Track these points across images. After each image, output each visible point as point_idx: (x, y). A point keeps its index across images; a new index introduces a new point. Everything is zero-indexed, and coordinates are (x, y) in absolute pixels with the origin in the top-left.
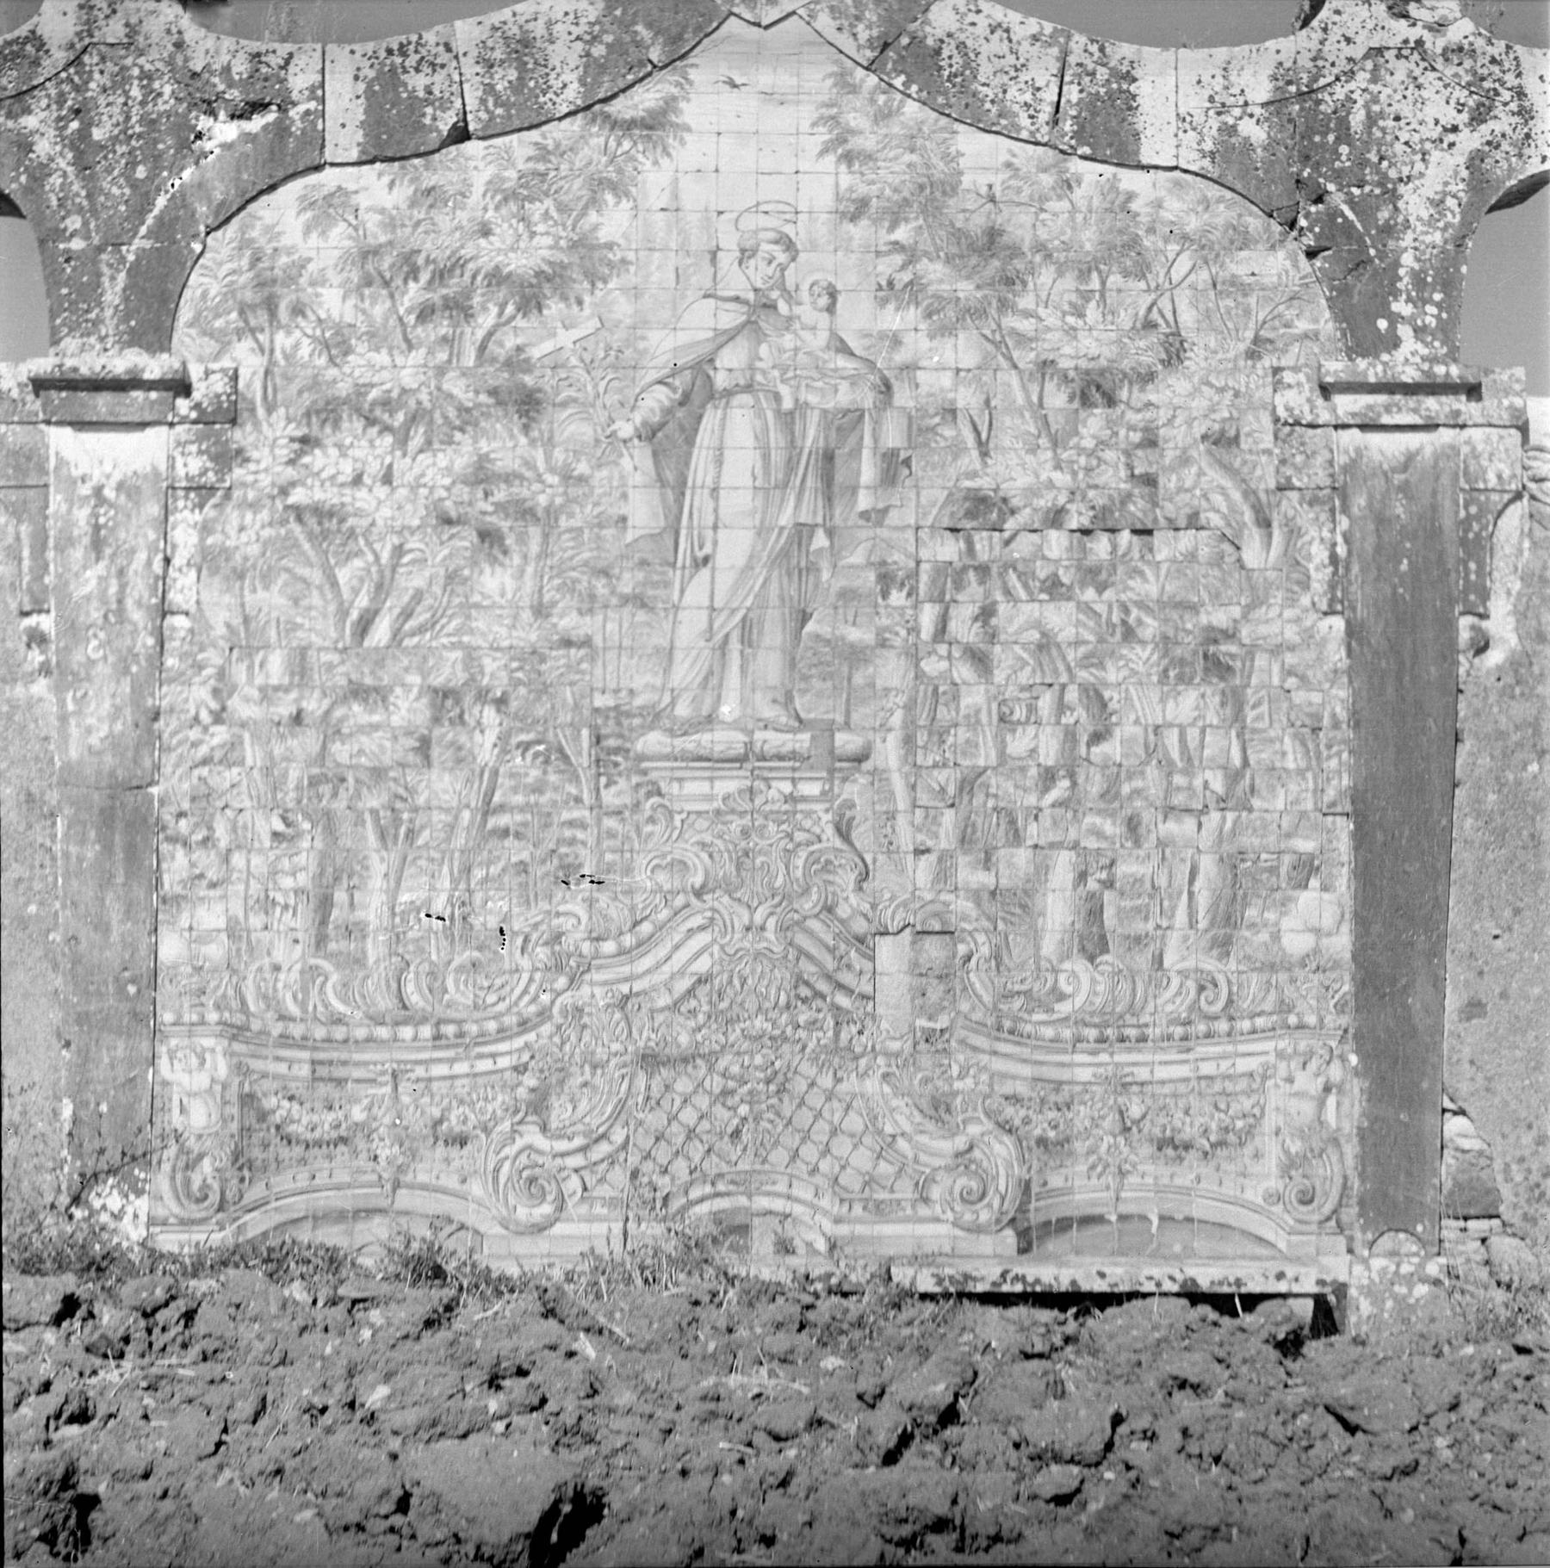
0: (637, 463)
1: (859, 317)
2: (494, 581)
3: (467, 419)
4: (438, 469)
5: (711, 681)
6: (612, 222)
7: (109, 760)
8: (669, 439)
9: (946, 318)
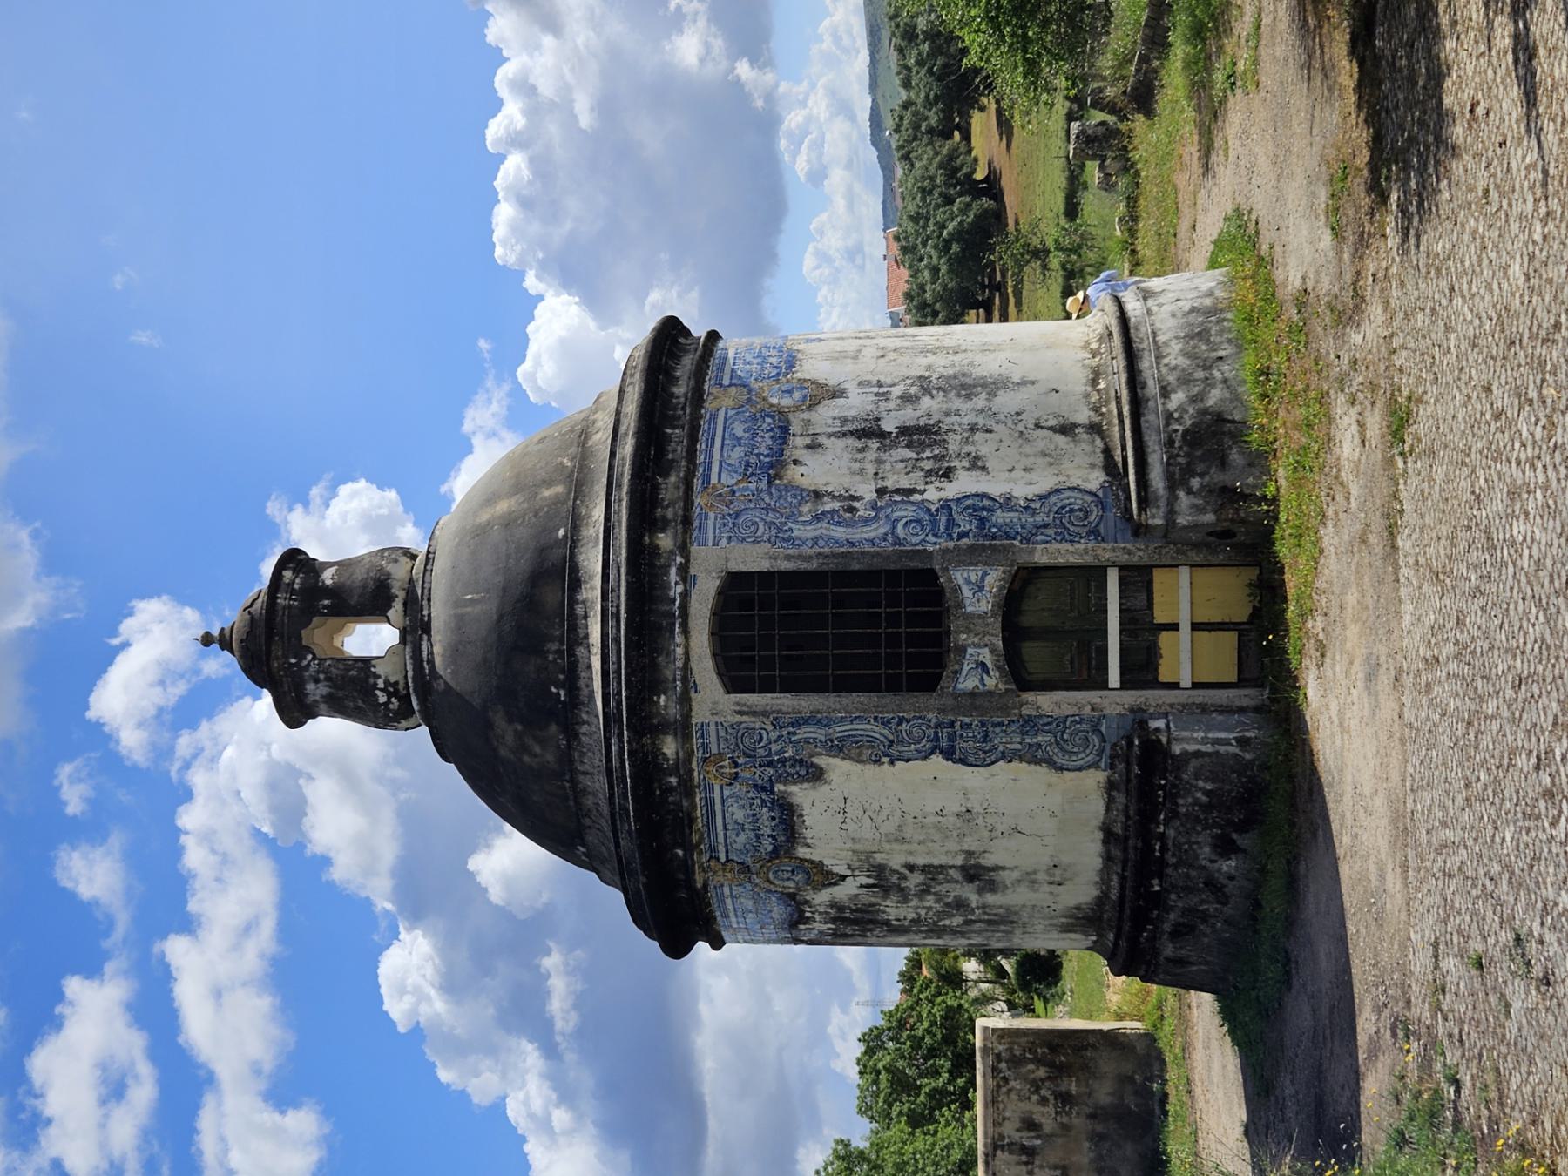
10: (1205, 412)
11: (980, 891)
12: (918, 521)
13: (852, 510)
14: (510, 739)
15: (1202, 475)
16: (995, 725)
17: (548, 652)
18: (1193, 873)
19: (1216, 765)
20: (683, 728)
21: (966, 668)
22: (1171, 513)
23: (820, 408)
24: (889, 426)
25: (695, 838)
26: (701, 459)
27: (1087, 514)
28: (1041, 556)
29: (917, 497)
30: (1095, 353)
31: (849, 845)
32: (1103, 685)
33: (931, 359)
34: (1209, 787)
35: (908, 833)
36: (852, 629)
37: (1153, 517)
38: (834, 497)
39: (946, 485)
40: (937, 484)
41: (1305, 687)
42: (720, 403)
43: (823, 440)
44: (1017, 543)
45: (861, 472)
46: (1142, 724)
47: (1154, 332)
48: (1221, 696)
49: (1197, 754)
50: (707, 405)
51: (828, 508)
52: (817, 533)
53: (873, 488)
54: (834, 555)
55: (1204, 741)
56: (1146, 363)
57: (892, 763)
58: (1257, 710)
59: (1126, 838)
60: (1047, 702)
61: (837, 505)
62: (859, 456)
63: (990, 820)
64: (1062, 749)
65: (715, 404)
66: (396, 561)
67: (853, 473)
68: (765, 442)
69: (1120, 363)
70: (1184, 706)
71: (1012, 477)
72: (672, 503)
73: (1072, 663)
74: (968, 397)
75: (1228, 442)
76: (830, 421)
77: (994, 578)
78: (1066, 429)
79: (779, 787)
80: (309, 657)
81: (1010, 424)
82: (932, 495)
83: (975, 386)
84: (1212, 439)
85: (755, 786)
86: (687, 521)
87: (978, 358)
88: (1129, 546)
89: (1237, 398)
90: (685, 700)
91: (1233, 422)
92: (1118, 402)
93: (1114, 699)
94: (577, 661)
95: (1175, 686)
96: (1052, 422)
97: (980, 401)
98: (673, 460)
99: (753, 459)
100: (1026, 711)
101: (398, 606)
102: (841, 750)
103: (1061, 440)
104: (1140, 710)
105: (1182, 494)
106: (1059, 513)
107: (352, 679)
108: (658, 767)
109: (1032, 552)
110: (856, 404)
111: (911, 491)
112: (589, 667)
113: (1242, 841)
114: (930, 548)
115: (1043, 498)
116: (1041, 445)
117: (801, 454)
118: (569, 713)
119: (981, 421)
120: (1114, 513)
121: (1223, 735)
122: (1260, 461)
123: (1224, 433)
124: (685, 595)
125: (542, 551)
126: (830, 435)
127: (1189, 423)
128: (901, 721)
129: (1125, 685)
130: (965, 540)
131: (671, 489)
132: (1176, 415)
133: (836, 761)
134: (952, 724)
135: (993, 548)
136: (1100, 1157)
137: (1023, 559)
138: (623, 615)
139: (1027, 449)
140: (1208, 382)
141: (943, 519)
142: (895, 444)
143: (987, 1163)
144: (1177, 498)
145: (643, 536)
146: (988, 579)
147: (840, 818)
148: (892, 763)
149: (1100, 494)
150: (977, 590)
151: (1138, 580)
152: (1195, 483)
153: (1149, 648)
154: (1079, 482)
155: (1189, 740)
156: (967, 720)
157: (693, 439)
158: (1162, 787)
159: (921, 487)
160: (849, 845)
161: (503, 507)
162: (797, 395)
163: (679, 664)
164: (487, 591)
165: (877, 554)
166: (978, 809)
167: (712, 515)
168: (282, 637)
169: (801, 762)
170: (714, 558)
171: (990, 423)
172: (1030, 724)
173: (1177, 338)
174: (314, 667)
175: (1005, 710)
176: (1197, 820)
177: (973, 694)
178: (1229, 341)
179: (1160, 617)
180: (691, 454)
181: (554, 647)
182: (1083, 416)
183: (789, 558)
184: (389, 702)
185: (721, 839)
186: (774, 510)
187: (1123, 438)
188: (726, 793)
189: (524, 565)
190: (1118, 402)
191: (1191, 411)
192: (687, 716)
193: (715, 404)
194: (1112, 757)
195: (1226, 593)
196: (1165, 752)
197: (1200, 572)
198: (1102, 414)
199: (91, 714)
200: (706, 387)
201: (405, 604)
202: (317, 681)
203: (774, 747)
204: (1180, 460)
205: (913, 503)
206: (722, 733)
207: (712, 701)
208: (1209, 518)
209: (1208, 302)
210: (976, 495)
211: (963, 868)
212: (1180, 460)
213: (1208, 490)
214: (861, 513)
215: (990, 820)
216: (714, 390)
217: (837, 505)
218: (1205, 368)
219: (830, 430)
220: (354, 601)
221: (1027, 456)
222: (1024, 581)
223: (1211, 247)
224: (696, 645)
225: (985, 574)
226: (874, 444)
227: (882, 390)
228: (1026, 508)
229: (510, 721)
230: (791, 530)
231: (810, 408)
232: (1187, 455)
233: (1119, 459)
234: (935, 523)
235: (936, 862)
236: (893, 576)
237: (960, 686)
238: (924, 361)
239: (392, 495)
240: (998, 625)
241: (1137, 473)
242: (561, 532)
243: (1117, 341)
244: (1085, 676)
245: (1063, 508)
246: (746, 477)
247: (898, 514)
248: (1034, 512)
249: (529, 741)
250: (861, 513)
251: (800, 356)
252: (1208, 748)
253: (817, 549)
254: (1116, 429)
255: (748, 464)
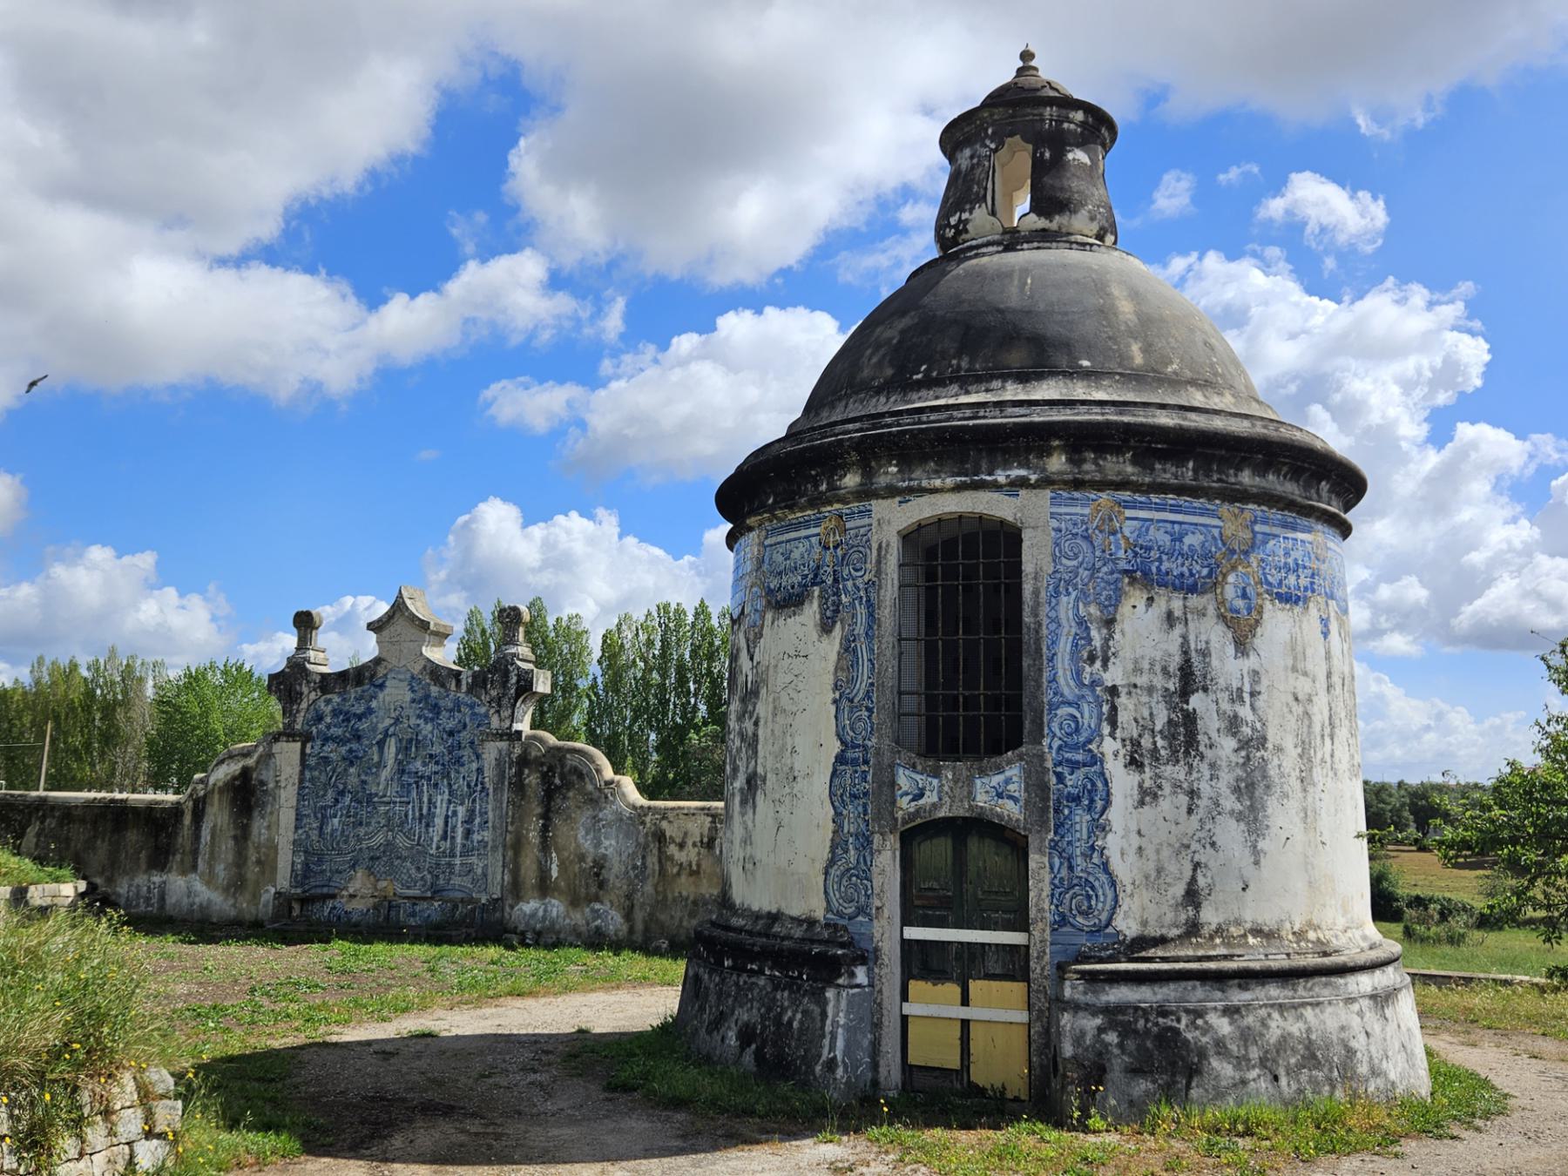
0: (375, 749)
1: (413, 721)
2: (352, 770)
3: (349, 741)
4: (343, 750)
5: (386, 789)
6: (374, 704)
7: (1158, 466)
8: (381, 744)
9: (426, 720)
10: (1202, 1054)
11: (741, 790)
12: (1077, 730)
13: (1092, 659)
14: (888, 334)
15: (1121, 1045)
16: (865, 806)
17: (960, 358)
18: (730, 1001)
19: (813, 1033)
20: (866, 493)
21: (918, 777)
22: (1076, 1007)
23: (1221, 628)
24: (1196, 701)
25: (779, 513)
26: (1155, 498)
27: (1085, 914)
28: (1034, 860)
29: (1106, 729)
30: (1300, 935)
31: (773, 662)
32: (907, 921)
33: (1292, 752)
34: (795, 1024)
35: (780, 719)
36: (969, 661)
37: (1073, 987)
38: (1107, 640)
39: (1121, 760)
40: (1122, 752)
41: (839, 1143)
42: (1228, 521)
43: (1179, 630)
44: (1051, 835)
45: (1137, 670)
46: (862, 960)
47: (1318, 1004)
48: (891, 1045)
49: (824, 1015)
50: (1226, 506)
51: (1094, 633)
52: (1064, 622)
53: (1118, 682)
54: (1038, 641)
55: (835, 1023)
56: (1274, 991)
57: (835, 701)
58: (875, 1083)
59: (767, 936)
60: (887, 863)
61: (1097, 643)
62: (1158, 668)
63: (787, 800)
64: (843, 875)
65: (1226, 514)
66: (1092, 219)
67: (1136, 662)
68: (1172, 566)
69: (1278, 962)
70: (880, 1005)
71: (1132, 835)
72: (1100, 469)
73: (930, 889)
74: (1236, 790)
75: (1163, 1079)
76: (1203, 638)
77: (1011, 810)
78: (1192, 896)
79: (816, 590)
80: (993, 146)
81: (1199, 834)
82: (1109, 746)
83: (1251, 798)
84: (1169, 1062)
85: (818, 567)
86: (1078, 484)
87: (1293, 805)
88: (1047, 958)
89: (1220, 1095)
90: (891, 492)
91: (1188, 1087)
92: (1225, 957)
93: (888, 932)
94: (945, 386)
95: (905, 997)
96: (1201, 882)
97: (1229, 803)
98: (1153, 469)
99: (1154, 554)
100: (877, 838)
101: (1042, 223)
102: (846, 650)
103: (1179, 890)
104: (877, 958)
105: (1098, 1021)
106: (1088, 883)
107: (970, 189)
108: (833, 471)
109: (1041, 851)
110: (1227, 667)
111: (1113, 723)
112: (937, 398)
113: (748, 1058)
114: (1045, 742)
115: (1105, 867)
116: (1172, 868)
117: (1161, 606)
118: (902, 384)
119: (1203, 803)
120: (1084, 943)
121: (840, 1043)
122: (1135, 1115)
123: (1173, 1075)
124: (996, 486)
125: (1066, 346)
126: (1185, 637)
127: (1189, 1036)
128: (869, 710)
129: (907, 945)
130: (1054, 780)
131: (1117, 468)
132: (1200, 1022)
133: (837, 647)
134: (866, 762)
135: (1045, 810)
136: (706, 903)
137: (1033, 842)
138: (971, 423)
139: (1166, 853)
140: (1241, 1062)
141: (1079, 757)
142: (1172, 708)
143: (703, 809)
144: (1094, 1014)
145: (1060, 438)
146: (1010, 804)
147: (792, 653)
148: (835, 701)
149: (1110, 930)
150: (998, 791)
151: (1014, 964)
152: (1112, 1038)
153: (944, 972)
154: (1125, 907)
155: (838, 1006)
156: (869, 778)
157: (1180, 490)
158: (800, 975)
159: (1118, 733)
160: (773, 662)
161: (1126, 308)
162: (1240, 603)
163: (925, 483)
164: (1031, 297)
165: (1039, 686)
166: (797, 787)
167: (1087, 511)
168: (1012, 116)
169: (837, 611)
170: (1040, 518)
171: (1201, 813)
172: (865, 842)
173: (1309, 1030)
174: (984, 152)
175: (878, 817)
176: (769, 1009)
177: (893, 784)
178: (1300, 1091)
179: (975, 986)
180: (1162, 488)
181: (964, 364)
182: (1210, 916)
183: (1036, 593)
184: (951, 227)
185: (780, 538)
186: (1092, 576)
187: (1177, 960)
188: (813, 540)
189: (1052, 329)
190: (1225, 957)
191: (1204, 1040)
192: (876, 495)
193: (1226, 514)
194: (835, 925)
195: (1002, 1063)
196: (830, 982)
197: (1023, 1032)
198: (1212, 938)
199: (1293, 176)
200: (1250, 506)
201: (1044, 230)
202: (972, 157)
203: (849, 584)
204: (1141, 1022)
205: (1099, 725)
206: (862, 531)
207: (892, 519)
208: (1068, 1050)
209: (1363, 1069)
210: (1108, 794)
211: (755, 773)
212: (1141, 1022)
213: (1102, 1051)
214: (1088, 669)
215: (787, 800)
216: (1247, 515)
217: (1097, 643)
218: (1263, 1063)
219: (1192, 638)
220: (1048, 180)
221: (1158, 852)
222: (1013, 842)
223: (1483, 1076)
224: (943, 500)
225: (1015, 800)
226: (1173, 685)
227: (1246, 697)
228: (1092, 848)
229: (902, 332)
230: (1069, 594)
231: (1222, 617)
232: (1147, 1031)
233: (1151, 953)
234: (1075, 747)
235: (760, 747)
236: (1015, 703)
237: (901, 771)
238: (1289, 743)
239: (1478, 383)
240: (961, 813)
241: (1127, 972)
242: (1086, 363)
243: (1312, 961)
244: (917, 902)
245: (1093, 888)
246: (1132, 546)
247: (1086, 708)
248: (1087, 856)
249: (882, 351)
250: (1088, 669)
251: (1297, 609)
252: (828, 1028)
253: (1045, 621)
254: (1190, 953)
255: (1149, 549)
